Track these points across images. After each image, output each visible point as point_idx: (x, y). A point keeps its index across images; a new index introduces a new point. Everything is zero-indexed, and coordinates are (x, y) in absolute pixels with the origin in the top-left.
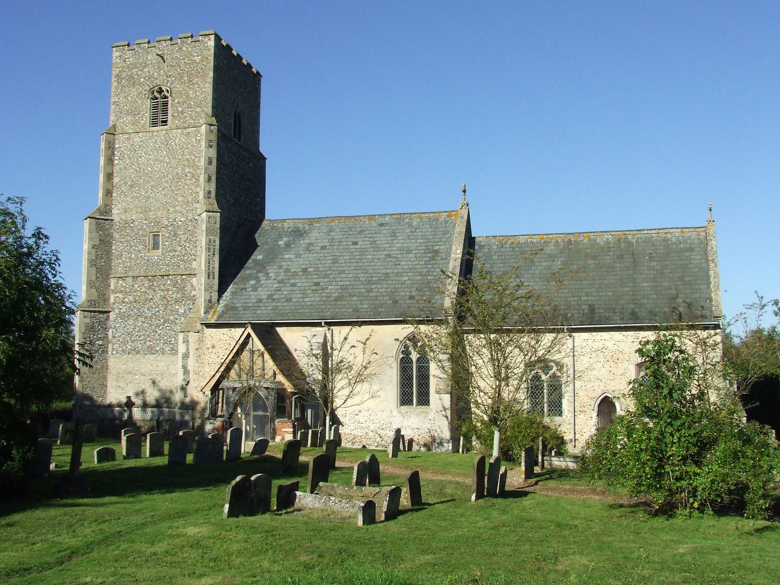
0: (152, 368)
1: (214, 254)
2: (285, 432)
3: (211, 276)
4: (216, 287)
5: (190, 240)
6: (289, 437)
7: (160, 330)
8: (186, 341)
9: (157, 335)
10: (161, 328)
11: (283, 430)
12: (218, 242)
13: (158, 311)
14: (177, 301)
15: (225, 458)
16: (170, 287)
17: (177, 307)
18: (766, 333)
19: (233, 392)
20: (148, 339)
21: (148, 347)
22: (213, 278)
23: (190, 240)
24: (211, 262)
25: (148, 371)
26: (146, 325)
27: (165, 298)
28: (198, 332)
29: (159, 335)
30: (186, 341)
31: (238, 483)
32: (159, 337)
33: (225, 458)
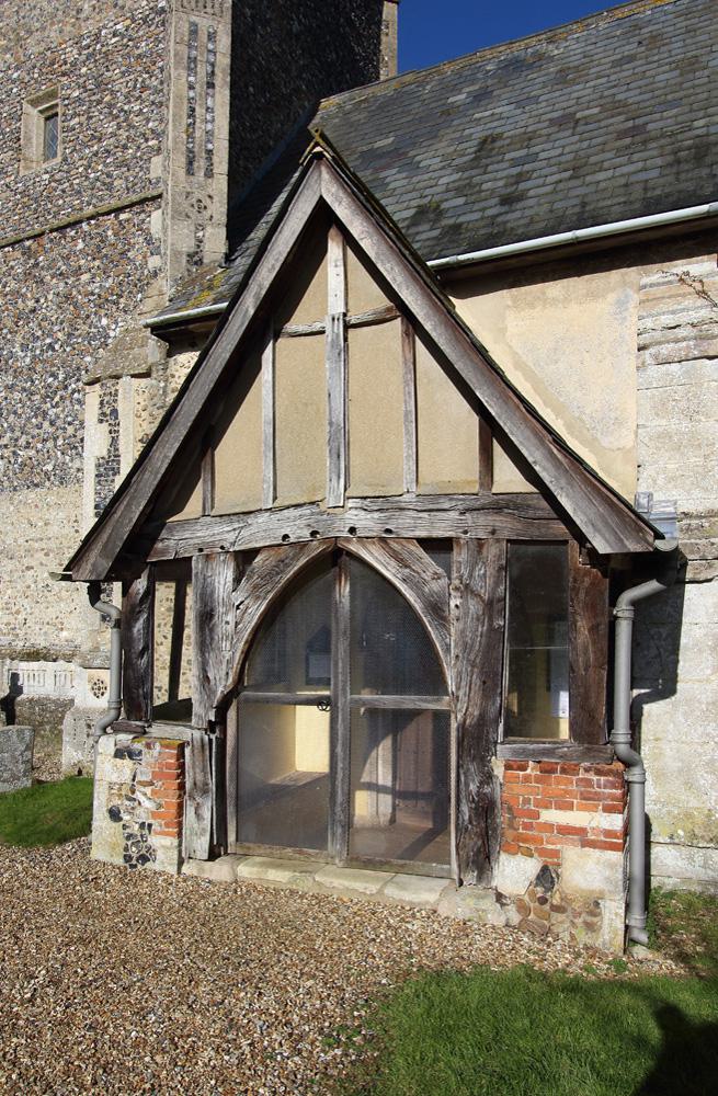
0: (32, 533)
1: (211, 85)
2: (566, 830)
3: (201, 163)
4: (219, 209)
5: (144, 88)
6: (562, 423)
7: (56, 406)
8: (109, 415)
9: (46, 424)
10: (57, 399)
11: (551, 816)
12: (224, 42)
13: (51, 347)
14: (102, 302)
15: (647, 691)
16: (82, 262)
17: (104, 321)
18: (265, 727)
19: (237, 581)
20: (22, 441)
21: (23, 465)
22: (209, 174)
23: (144, 88)
24: (199, 111)
25: (21, 541)
26: (17, 396)
27: (68, 297)
28: (147, 375)
29: (52, 423)
30: (109, 415)
31: (548, 757)
32: (51, 430)
33: (647, 691)
